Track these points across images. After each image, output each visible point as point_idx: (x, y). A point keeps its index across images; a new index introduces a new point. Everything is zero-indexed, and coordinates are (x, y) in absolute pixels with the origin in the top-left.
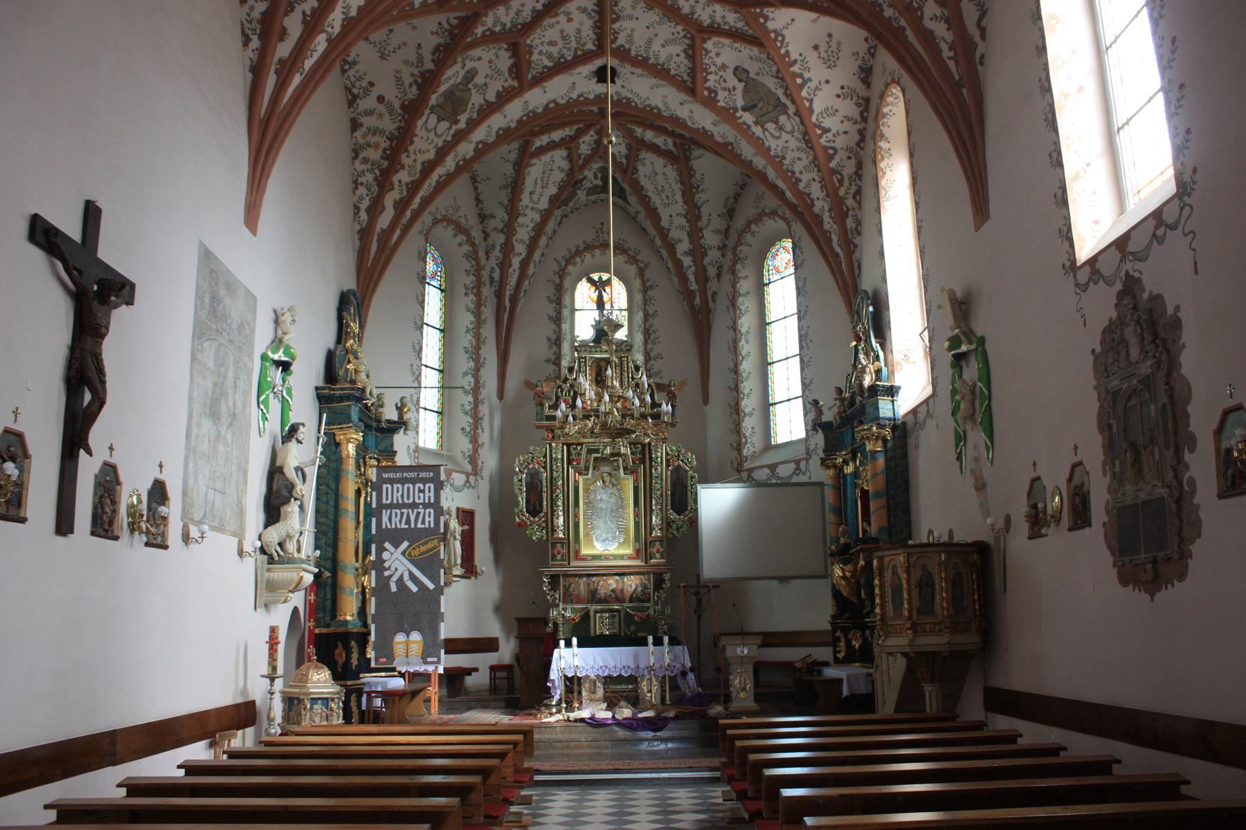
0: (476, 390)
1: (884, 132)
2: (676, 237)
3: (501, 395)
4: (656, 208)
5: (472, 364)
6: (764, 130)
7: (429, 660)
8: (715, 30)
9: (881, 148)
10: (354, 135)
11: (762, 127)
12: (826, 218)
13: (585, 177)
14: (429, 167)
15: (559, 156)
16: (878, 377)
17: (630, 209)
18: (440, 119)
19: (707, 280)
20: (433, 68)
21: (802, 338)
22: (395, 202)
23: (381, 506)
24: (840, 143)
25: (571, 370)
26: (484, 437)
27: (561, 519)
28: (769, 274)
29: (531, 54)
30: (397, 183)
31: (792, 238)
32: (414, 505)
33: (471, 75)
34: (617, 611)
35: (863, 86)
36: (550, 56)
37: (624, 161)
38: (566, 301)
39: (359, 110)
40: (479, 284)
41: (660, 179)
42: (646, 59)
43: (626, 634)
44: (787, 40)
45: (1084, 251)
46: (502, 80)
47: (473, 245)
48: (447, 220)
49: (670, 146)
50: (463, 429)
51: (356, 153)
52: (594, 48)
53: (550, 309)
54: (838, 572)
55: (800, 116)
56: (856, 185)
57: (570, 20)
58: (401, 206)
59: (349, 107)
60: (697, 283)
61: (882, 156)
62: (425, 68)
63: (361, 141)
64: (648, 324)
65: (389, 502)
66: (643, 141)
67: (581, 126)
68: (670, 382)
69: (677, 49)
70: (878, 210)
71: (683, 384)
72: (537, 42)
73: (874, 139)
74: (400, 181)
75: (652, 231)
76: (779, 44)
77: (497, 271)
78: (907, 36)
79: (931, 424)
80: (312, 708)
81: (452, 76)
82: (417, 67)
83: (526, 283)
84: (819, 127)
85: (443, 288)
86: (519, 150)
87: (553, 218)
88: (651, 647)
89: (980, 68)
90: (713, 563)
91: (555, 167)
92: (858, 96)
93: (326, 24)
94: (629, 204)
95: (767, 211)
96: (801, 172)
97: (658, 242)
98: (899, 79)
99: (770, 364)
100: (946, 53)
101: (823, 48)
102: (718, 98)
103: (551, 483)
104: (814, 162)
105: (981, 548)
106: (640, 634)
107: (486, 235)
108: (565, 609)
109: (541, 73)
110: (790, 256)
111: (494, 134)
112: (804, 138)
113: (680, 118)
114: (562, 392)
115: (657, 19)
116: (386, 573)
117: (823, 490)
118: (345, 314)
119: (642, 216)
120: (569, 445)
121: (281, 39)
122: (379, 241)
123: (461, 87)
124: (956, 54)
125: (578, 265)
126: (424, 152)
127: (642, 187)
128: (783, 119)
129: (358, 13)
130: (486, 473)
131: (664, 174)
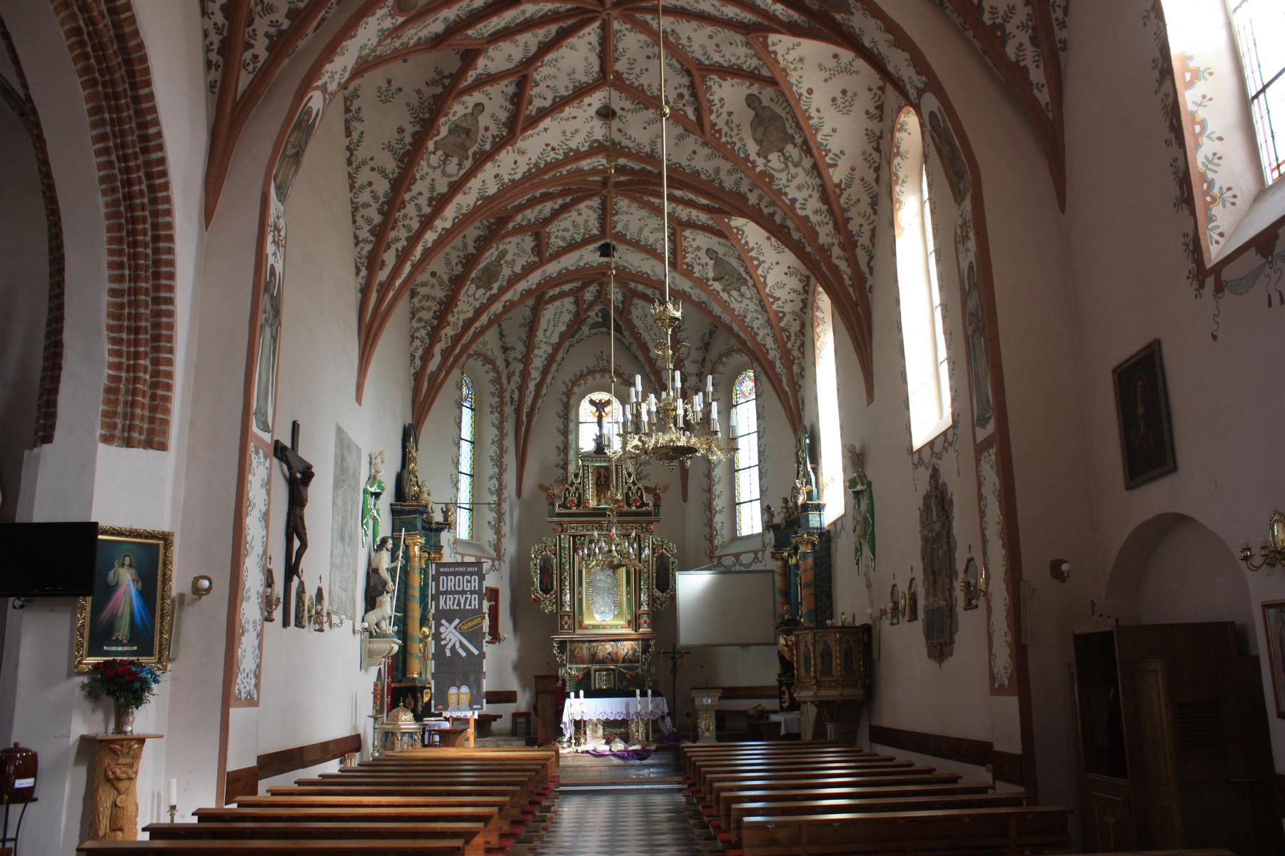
0: (499, 491)
4: (646, 343)
5: (497, 470)
6: (730, 296)
7: (475, 707)
8: (691, 225)
9: (817, 316)
10: (413, 300)
11: (728, 293)
12: (778, 364)
14: (468, 323)
15: (568, 303)
17: (625, 341)
20: (475, 252)
21: (760, 416)
22: (442, 350)
23: (439, 593)
25: (576, 476)
26: (506, 529)
27: (568, 596)
32: (463, 592)
33: (503, 254)
34: (613, 670)
36: (564, 239)
37: (620, 305)
38: (572, 416)
40: (502, 403)
43: (619, 688)
45: (919, 440)
48: (478, 354)
50: (489, 523)
51: (413, 314)
52: (598, 233)
53: (559, 423)
54: (782, 641)
55: (756, 288)
57: (580, 214)
58: (446, 353)
62: (469, 251)
63: (417, 305)
65: (445, 589)
66: (636, 291)
68: (656, 486)
71: (666, 488)
73: (812, 308)
74: (446, 335)
76: (740, 237)
77: (517, 392)
79: (843, 535)
80: (402, 739)
81: (490, 255)
82: (462, 251)
83: (540, 401)
88: (638, 698)
90: (688, 631)
91: (564, 310)
92: (801, 274)
99: (737, 471)
100: (847, 282)
102: (694, 271)
103: (560, 567)
105: (867, 629)
106: (631, 689)
107: (508, 363)
108: (571, 669)
109: (557, 252)
111: (519, 295)
114: (569, 493)
116: (443, 643)
117: (773, 576)
119: (634, 347)
120: (574, 537)
121: (381, 269)
122: (429, 380)
123: (495, 263)
127: (635, 325)
128: (744, 289)
130: (507, 558)
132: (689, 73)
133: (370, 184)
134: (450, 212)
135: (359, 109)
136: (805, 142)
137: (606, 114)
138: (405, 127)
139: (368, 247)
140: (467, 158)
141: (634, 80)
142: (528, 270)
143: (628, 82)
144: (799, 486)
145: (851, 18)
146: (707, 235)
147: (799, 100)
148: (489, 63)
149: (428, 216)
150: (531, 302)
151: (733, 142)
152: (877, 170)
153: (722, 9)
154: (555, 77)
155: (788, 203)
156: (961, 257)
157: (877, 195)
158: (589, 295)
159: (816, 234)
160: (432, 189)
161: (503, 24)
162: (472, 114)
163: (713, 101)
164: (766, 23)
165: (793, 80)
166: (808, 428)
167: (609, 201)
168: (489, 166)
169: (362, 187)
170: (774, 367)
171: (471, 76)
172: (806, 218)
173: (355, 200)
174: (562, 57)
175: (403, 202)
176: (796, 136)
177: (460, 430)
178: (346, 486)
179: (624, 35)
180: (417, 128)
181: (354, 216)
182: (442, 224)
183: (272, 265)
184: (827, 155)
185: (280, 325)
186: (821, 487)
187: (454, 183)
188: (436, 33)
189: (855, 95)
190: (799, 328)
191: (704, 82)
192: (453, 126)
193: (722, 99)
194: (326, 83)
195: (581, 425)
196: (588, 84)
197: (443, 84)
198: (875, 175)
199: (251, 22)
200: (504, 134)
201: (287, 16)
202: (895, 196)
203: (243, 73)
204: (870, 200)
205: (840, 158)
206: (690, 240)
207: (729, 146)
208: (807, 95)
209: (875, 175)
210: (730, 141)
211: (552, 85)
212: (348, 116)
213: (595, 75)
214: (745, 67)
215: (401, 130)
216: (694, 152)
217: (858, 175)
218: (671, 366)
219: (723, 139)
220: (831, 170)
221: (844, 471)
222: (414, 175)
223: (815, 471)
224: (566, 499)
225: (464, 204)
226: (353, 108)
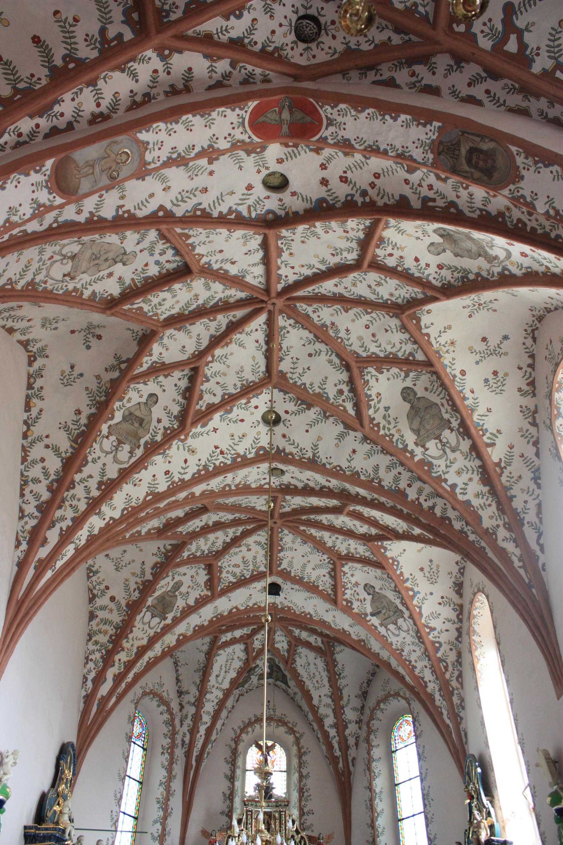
1: (476, 629)
2: (324, 713)
4: (309, 691)
5: (161, 813)
6: (388, 630)
8: (350, 558)
9: (474, 641)
10: (91, 623)
11: (386, 627)
12: (437, 696)
13: (258, 666)
14: (142, 651)
15: (239, 648)
16: (493, 834)
17: (290, 691)
18: (153, 616)
19: (348, 747)
21: (421, 757)
22: (115, 675)
24: (444, 638)
28: (397, 744)
29: (221, 572)
30: (118, 661)
31: (412, 714)
33: (178, 586)
35: (458, 596)
36: (234, 575)
37: (286, 654)
38: (239, 763)
39: (96, 606)
40: (173, 746)
41: (312, 667)
42: (301, 579)
44: (400, 565)
46: (200, 590)
47: (171, 714)
48: (153, 694)
49: (320, 644)
51: (90, 637)
53: (226, 769)
56: (458, 670)
57: (249, 550)
59: (90, 603)
60: (340, 751)
61: (476, 646)
62: (146, 578)
63: (95, 628)
64: (302, 783)
67: (255, 627)
68: (319, 835)
69: (324, 571)
70: (476, 688)
71: (330, 837)
72: (225, 564)
73: (468, 634)
74: (120, 660)
75: (306, 708)
76: (395, 567)
77: (188, 735)
78: (487, 553)
83: (210, 746)
84: (428, 627)
85: (145, 747)
86: (210, 643)
87: (233, 696)
89: (542, 572)
91: (235, 657)
93: (76, 537)
94: (289, 687)
95: (392, 693)
96: (416, 661)
97: (310, 716)
98: (483, 589)
100: (517, 564)
101: (427, 569)
104: (425, 653)
107: (182, 707)
110: (411, 728)
111: (192, 629)
112: (416, 635)
113: (326, 622)
115: (310, 550)
118: (62, 762)
121: (43, 545)
122: (99, 705)
123: (170, 594)
124: (524, 563)
125: (250, 734)
126: (139, 639)
127: (299, 674)
128: (400, 621)
129: (99, 532)
131: (315, 664)
132: (348, 368)
133: (43, 460)
135: (42, 388)
136: (463, 424)
138: (81, 409)
139: (33, 522)
140: (139, 447)
141: (297, 380)
143: (291, 381)
145: (522, 184)
147: (454, 380)
148: (164, 351)
149: (96, 499)
151: (391, 434)
152: (536, 443)
154: (225, 374)
155: (449, 489)
157: (539, 469)
159: (479, 518)
160: (103, 474)
162: (146, 404)
163: (370, 396)
165: (446, 362)
168: (158, 459)
169: (34, 462)
170: (434, 700)
171: (146, 362)
172: (468, 502)
173: (26, 474)
174: (232, 354)
175: (73, 482)
176: (452, 420)
179: (288, 332)
180: (93, 410)
181: (22, 490)
184: (484, 435)
187: (125, 469)
189: (506, 375)
190: (456, 658)
193: (379, 394)
197: (120, 368)
198: (534, 449)
200: (175, 427)
204: (532, 475)
205: (497, 437)
206: (348, 575)
207: (387, 438)
208: (461, 376)
210: (388, 433)
212: (30, 392)
213: (262, 375)
214: (400, 354)
215: (78, 412)
216: (354, 451)
217: (516, 451)
219: (382, 432)
220: (489, 450)
222: (86, 457)
226: (36, 386)
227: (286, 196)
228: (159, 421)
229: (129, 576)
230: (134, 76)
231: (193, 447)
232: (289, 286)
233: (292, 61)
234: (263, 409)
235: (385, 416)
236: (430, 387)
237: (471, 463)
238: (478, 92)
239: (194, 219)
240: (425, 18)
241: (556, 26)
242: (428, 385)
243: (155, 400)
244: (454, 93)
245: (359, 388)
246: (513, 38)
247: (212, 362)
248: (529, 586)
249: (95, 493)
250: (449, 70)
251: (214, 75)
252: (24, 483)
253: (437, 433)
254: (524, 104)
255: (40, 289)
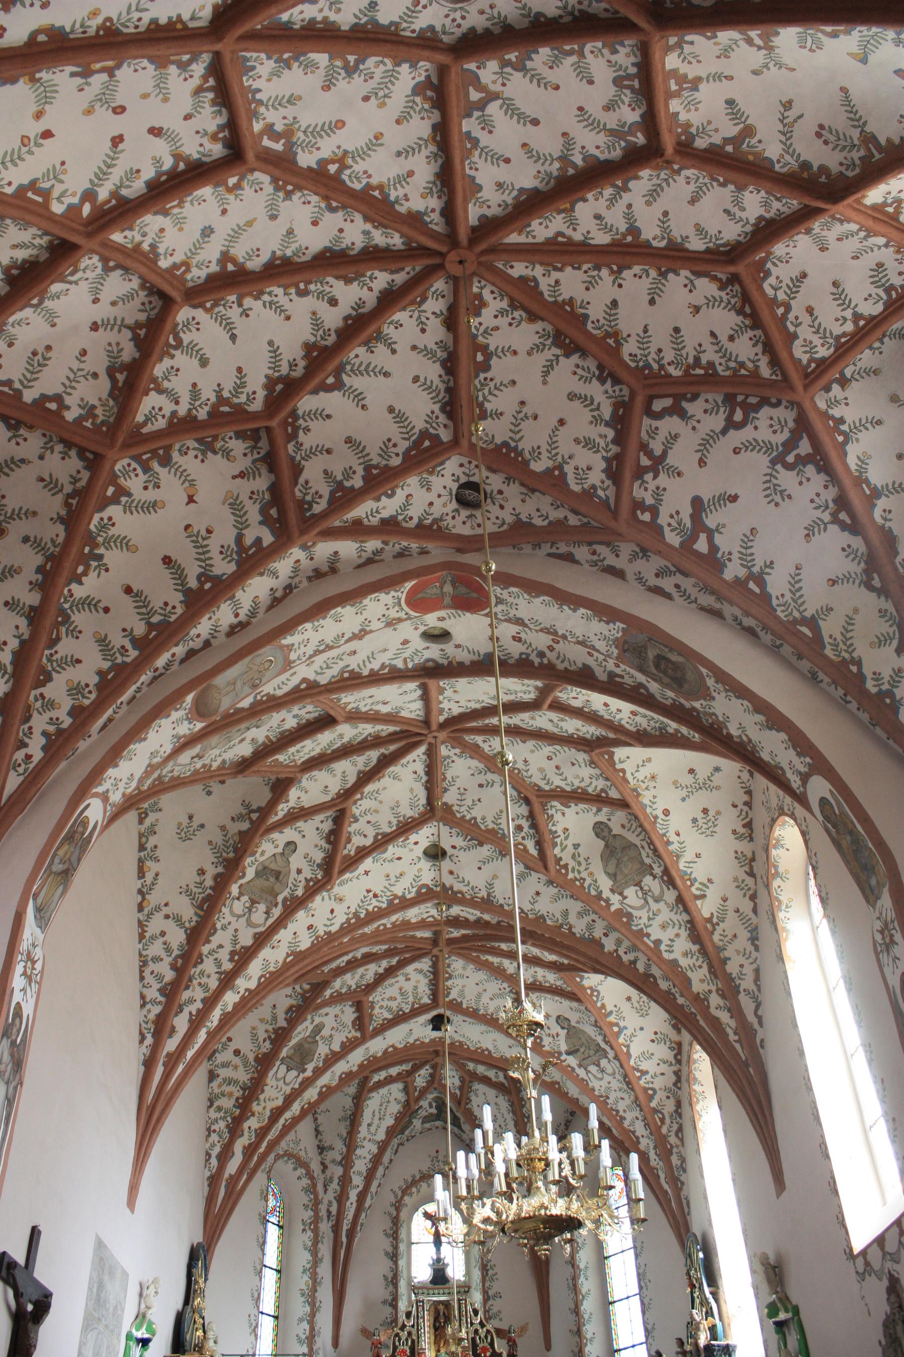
0: (311, 1338)
3: (336, 1343)
5: (308, 1309)
6: (588, 1072)
16: (714, 1337)
17: (464, 1136)
21: (640, 1277)
22: (244, 1148)
24: (658, 1083)
25: (408, 1315)
29: (373, 1008)
33: (318, 1029)
35: (675, 1032)
36: (390, 1010)
37: (458, 1092)
38: (403, 1235)
40: (316, 1220)
45: (859, 1242)
47: (312, 1178)
48: (288, 1155)
51: (211, 1102)
53: (386, 1243)
55: (619, 1060)
57: (408, 979)
58: (249, 1151)
63: (216, 1091)
70: (698, 1151)
71: (523, 1329)
72: (378, 998)
73: (688, 1081)
81: (303, 1030)
83: (363, 1215)
84: (638, 1070)
89: (761, 1050)
91: (392, 1099)
96: (624, 1111)
99: (611, 1303)
100: (732, 1037)
107: (325, 1167)
109: (382, 1025)
111: (337, 1078)
114: (399, 1341)
121: (170, 1036)
122: (227, 1187)
123: (309, 1040)
128: (604, 1062)
129: (234, 1008)
132: (527, 801)
133: (163, 934)
134: (255, 970)
135: (156, 847)
136: (666, 872)
137: (435, 854)
138: (205, 868)
139: (157, 1009)
140: (276, 905)
142: (349, 1047)
144: (698, 1318)
145: (713, 703)
146: (557, 998)
147: (655, 822)
148: (302, 795)
150: (352, 1090)
152: (753, 897)
153: (561, 724)
154: (376, 811)
156: (887, 971)
157: (756, 928)
158: (421, 1079)
159: (689, 981)
160: (235, 941)
161: (317, 751)
162: (283, 854)
163: (556, 832)
164: (611, 735)
165: (646, 801)
166: (699, 1239)
167: (440, 964)
168: (301, 915)
169: (153, 938)
171: (282, 809)
172: (675, 962)
173: (144, 953)
174: (385, 788)
175: (200, 956)
176: (655, 866)
177: (264, 1254)
178: (101, 1328)
180: (220, 869)
181: (141, 972)
182: (247, 981)
183: (18, 1003)
184: (692, 885)
185: (21, 1084)
186: (726, 1321)
187: (261, 934)
188: (242, 757)
189: (718, 813)
191: (544, 810)
192: (260, 868)
194: (108, 791)
195: (413, 1246)
196: (414, 819)
197: (250, 819)
199: (27, 719)
200: (319, 877)
201: (70, 714)
202: (780, 924)
203: (12, 774)
204: (749, 935)
209: (752, 904)
211: (373, 821)
212: (142, 854)
213: (422, 809)
214: (590, 790)
215: (202, 872)
216: (538, 893)
217: (731, 905)
218: (534, 1093)
219: (571, 876)
220: (699, 902)
221: (757, 1295)
222: (215, 924)
223: (715, 1295)
224: (395, 1348)
225: (272, 960)
226: (149, 846)
227: (449, 648)
228: (299, 871)
229: (257, 1023)
230: (275, 575)
231: (341, 895)
232: (454, 718)
233: (454, 531)
234: (424, 844)
235: (574, 854)
236: (628, 826)
237: (678, 917)
238: (667, 584)
239: (342, 684)
240: (605, 503)
241: (748, 534)
242: (625, 822)
243: (293, 848)
244: (640, 580)
245: (542, 827)
246: (703, 537)
247: (360, 799)
248: (747, 1066)
249: (228, 966)
250: (634, 557)
251: (363, 554)
252: (144, 964)
253: (637, 879)
254: (717, 606)
255: (167, 779)
